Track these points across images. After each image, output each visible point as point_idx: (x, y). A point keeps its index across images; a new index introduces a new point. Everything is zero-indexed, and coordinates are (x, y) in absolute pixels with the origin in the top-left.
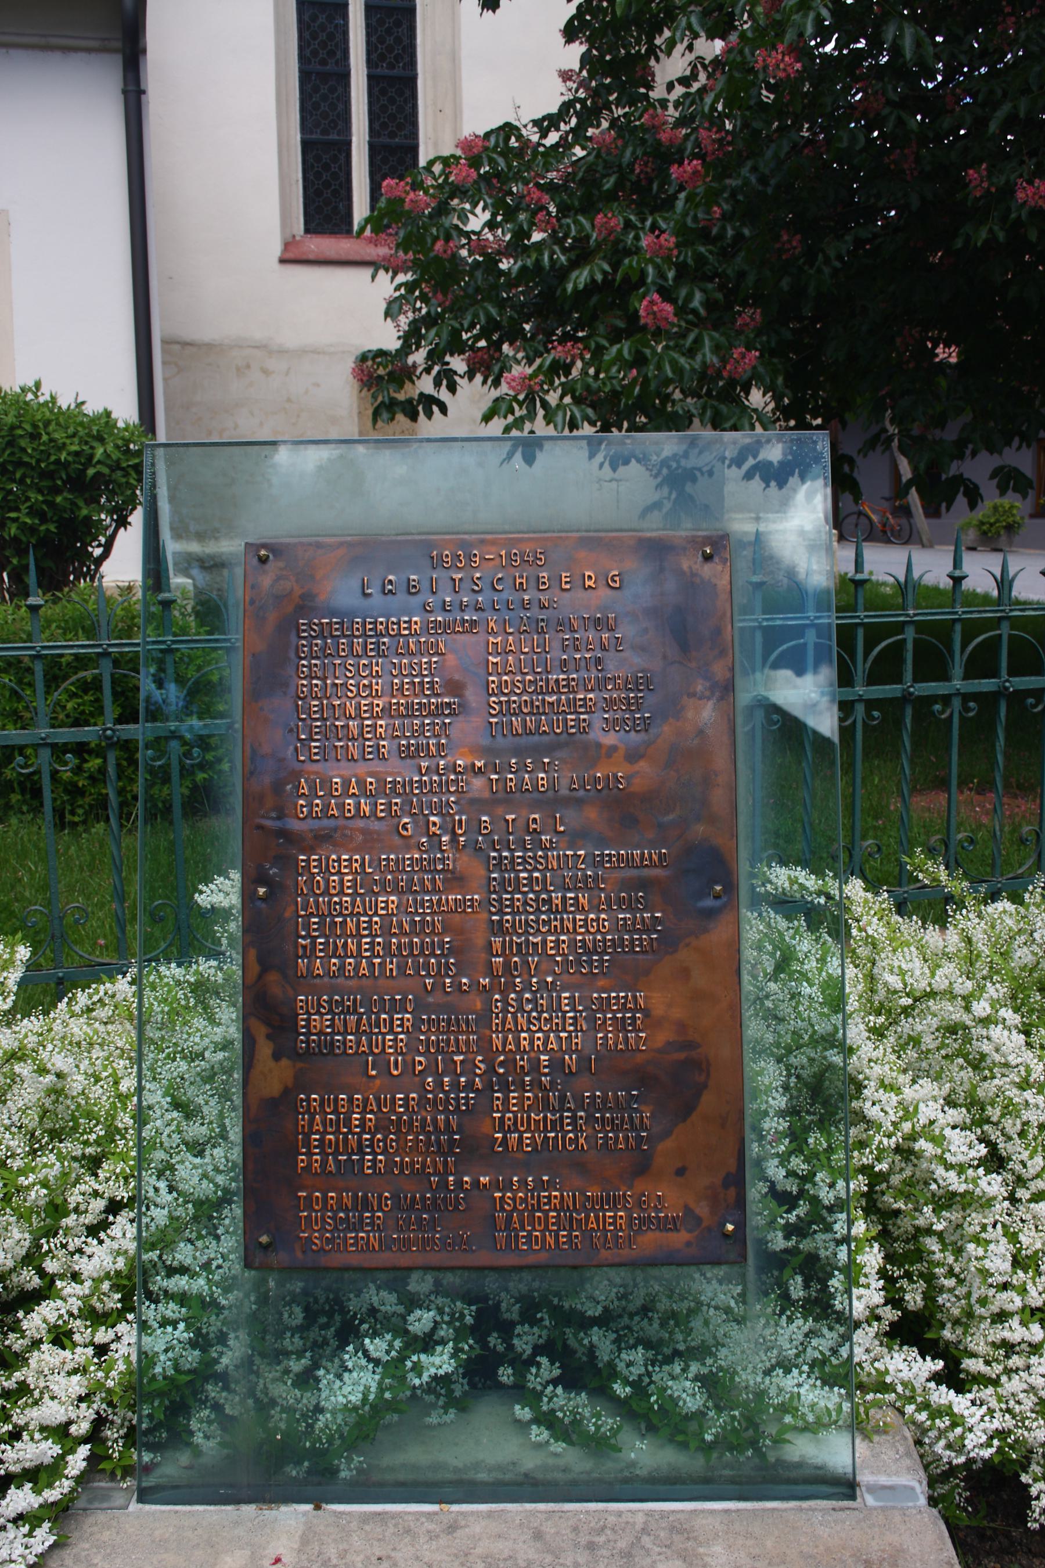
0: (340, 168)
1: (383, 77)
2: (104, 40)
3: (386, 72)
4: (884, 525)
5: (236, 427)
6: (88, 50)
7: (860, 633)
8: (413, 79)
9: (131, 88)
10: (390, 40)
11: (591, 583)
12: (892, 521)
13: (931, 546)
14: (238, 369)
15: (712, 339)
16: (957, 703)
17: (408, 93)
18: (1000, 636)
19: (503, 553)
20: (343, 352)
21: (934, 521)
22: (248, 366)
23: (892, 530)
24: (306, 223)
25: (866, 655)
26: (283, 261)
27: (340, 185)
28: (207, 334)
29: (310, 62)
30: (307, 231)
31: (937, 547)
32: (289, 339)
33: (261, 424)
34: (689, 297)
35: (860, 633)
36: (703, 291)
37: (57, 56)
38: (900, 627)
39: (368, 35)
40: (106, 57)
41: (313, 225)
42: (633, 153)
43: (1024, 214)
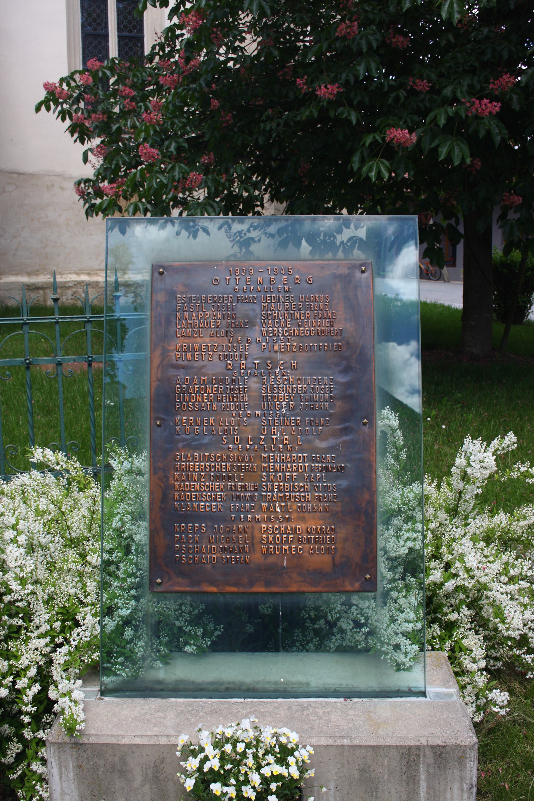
1: (126, 37)
3: (128, 34)
4: (427, 271)
5: (47, 217)
8: (143, 37)
12: (431, 268)
13: (449, 282)
14: (48, 187)
15: (180, 167)
22: (53, 186)
23: (431, 273)
28: (30, 169)
31: (452, 282)
33: (60, 215)
34: (169, 147)
36: (176, 142)
39: (118, 15)
43: (325, 104)
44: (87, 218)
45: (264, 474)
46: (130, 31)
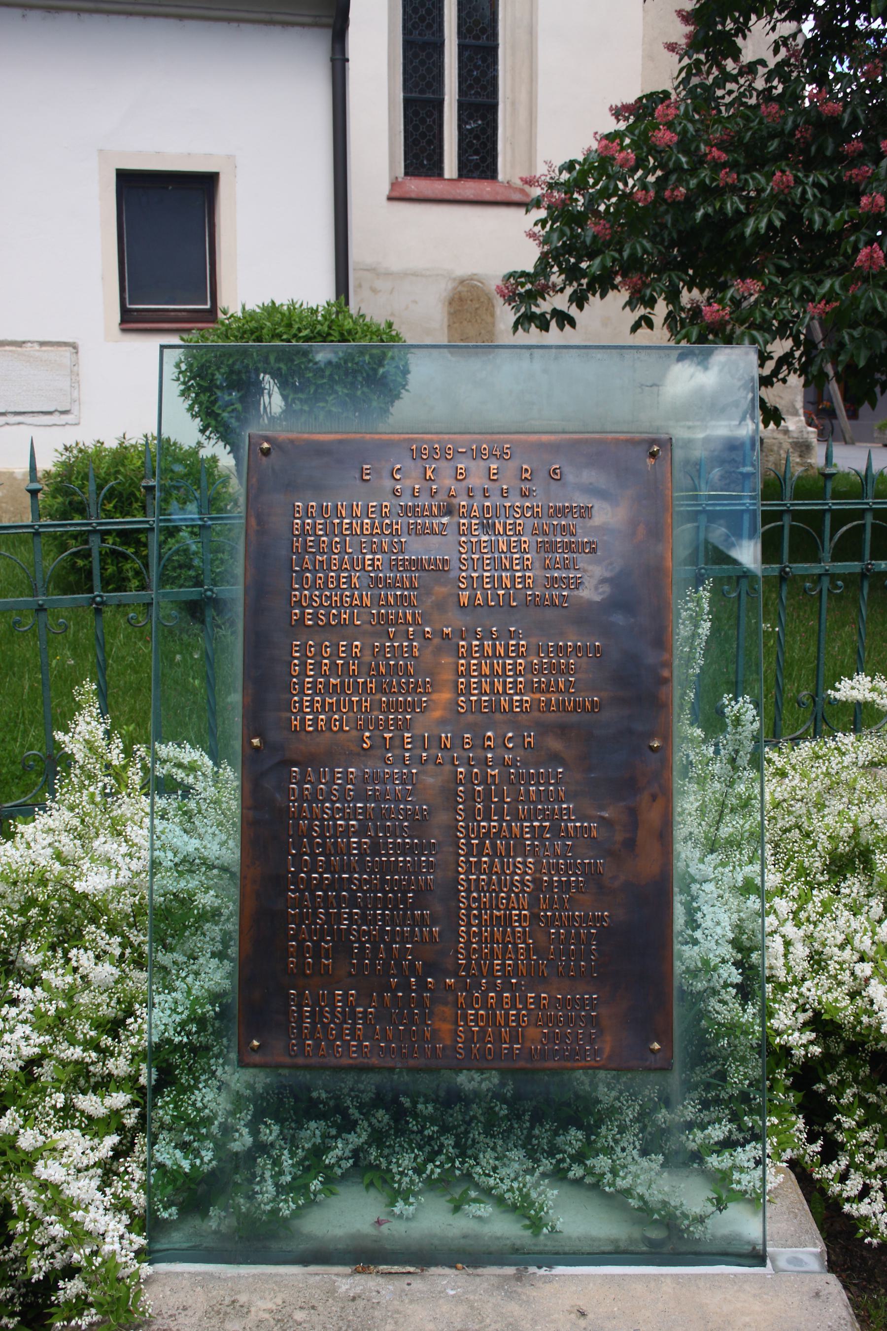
0: (434, 122)
2: (316, 16)
3: (473, 42)
6: (303, 25)
7: (828, 518)
8: (495, 49)
9: (338, 57)
10: (423, 12)
11: (527, 475)
13: (853, 443)
16: (826, 583)
17: (490, 60)
18: (782, 526)
19: (414, 447)
20: (437, 275)
21: (854, 422)
24: (406, 167)
25: (831, 539)
26: (390, 199)
27: (434, 136)
29: (411, 34)
30: (406, 174)
31: (858, 444)
32: (395, 264)
35: (828, 518)
37: (278, 29)
38: (861, 514)
39: (460, 11)
40: (317, 31)
41: (465, 172)
42: (794, 122)
44: (624, 308)
45: (461, 788)
46: (477, 37)
